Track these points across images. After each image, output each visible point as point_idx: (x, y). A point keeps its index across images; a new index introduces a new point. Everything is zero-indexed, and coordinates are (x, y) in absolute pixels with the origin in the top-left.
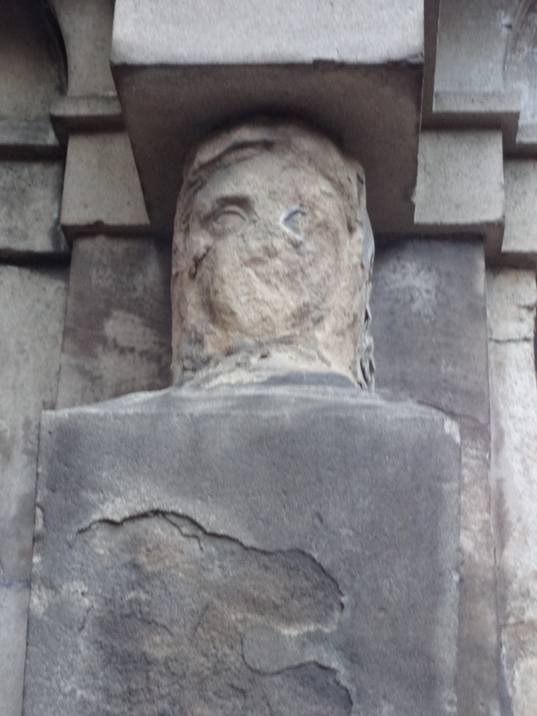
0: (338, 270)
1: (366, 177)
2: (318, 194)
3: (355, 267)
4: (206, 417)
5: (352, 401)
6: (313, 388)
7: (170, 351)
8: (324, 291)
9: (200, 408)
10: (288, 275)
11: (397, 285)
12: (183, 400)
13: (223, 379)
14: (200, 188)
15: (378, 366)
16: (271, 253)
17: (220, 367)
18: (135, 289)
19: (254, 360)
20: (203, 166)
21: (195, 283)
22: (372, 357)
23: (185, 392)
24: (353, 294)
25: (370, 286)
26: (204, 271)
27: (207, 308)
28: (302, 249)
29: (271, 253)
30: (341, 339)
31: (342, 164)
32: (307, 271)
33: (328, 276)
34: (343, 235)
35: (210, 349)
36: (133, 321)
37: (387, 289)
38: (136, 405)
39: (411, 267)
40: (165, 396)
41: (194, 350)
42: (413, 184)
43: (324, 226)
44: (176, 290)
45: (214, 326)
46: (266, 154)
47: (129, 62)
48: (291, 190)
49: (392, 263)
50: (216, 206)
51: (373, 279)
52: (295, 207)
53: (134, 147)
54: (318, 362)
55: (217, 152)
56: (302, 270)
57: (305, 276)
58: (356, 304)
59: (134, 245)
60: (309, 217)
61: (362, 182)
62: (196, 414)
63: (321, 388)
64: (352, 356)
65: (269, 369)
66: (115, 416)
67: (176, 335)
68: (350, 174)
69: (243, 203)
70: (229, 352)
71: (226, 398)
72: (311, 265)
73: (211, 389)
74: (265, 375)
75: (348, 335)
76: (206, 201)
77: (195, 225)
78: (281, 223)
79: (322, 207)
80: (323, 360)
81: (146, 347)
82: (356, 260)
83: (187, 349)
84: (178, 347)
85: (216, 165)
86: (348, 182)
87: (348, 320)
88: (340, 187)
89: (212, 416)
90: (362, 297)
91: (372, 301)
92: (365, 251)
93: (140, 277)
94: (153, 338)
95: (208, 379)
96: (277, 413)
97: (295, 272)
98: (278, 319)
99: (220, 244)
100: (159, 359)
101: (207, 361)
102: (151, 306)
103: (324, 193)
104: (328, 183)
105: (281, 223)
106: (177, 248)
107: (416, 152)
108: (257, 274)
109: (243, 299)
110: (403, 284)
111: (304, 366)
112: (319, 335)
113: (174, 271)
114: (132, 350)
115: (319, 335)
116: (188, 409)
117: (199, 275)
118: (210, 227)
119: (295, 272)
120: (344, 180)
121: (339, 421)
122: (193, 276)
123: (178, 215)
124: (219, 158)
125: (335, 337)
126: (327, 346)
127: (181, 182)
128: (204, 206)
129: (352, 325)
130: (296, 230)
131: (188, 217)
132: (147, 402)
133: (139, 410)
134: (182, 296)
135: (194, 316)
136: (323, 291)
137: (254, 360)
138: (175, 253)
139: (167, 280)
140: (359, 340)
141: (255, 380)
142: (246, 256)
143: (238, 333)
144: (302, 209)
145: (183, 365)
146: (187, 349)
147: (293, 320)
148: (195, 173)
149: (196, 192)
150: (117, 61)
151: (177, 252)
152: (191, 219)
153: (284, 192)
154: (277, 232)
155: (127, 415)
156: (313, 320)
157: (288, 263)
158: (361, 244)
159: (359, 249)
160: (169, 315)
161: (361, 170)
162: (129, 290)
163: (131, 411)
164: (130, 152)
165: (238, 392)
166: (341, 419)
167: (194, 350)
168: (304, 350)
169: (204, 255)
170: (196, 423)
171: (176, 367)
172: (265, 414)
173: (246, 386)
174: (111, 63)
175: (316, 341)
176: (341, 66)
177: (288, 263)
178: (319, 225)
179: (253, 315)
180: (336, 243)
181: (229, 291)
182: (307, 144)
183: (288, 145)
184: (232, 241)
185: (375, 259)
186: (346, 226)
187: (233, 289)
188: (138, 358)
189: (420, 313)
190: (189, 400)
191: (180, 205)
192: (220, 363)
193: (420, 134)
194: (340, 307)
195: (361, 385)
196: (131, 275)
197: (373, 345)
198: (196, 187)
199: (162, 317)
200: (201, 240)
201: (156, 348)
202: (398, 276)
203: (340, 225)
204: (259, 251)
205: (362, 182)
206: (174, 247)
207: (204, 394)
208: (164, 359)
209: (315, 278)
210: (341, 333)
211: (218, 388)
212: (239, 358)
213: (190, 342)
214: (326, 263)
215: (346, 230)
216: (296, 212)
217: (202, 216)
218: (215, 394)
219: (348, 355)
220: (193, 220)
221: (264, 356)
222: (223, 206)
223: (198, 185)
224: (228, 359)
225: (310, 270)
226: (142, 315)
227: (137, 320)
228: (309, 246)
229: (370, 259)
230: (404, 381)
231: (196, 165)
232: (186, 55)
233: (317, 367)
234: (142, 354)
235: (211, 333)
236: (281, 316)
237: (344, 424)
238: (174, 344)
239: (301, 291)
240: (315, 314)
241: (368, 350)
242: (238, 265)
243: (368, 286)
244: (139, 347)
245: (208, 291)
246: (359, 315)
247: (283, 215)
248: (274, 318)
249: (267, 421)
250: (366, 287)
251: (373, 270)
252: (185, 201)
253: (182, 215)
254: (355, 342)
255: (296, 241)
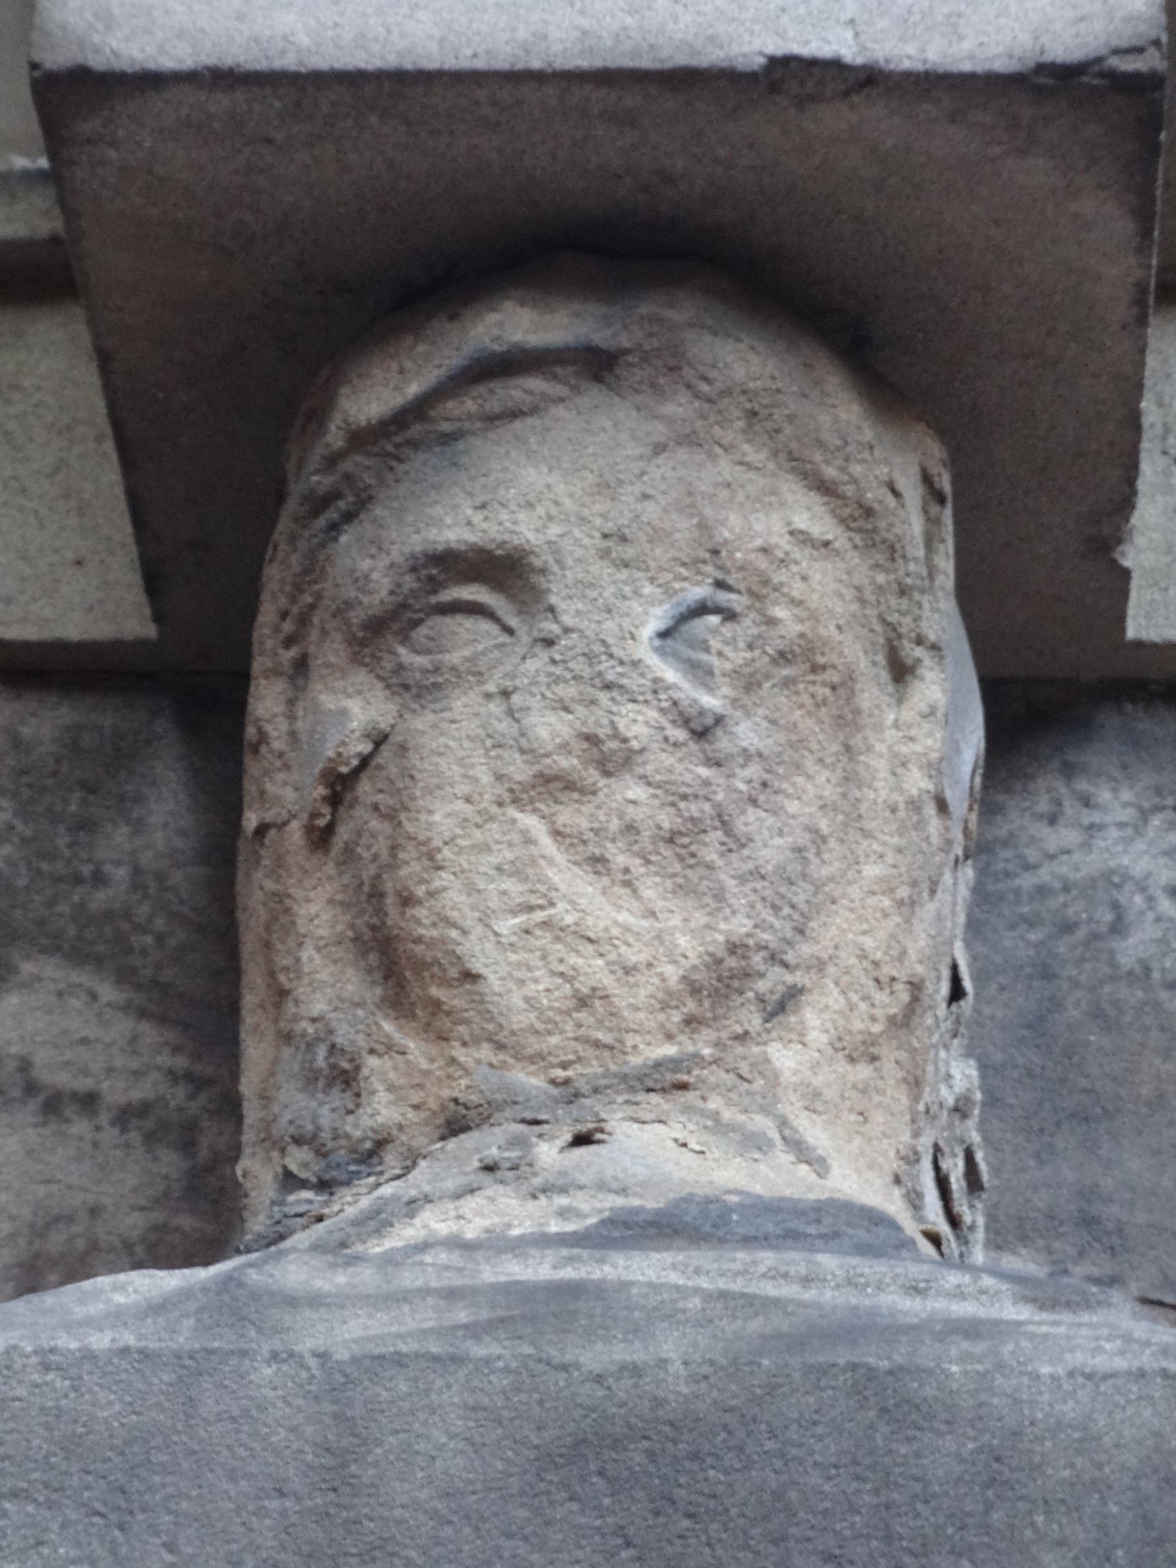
0: (853, 820)
1: (954, 483)
2: (784, 543)
3: (914, 805)
4: (378, 1363)
5: (911, 1307)
6: (767, 1258)
7: (230, 1107)
8: (801, 894)
9: (352, 1333)
10: (671, 840)
11: (1063, 868)
12: (291, 1301)
13: (434, 1222)
14: (349, 517)
15: (996, 1171)
16: (610, 757)
17: (421, 1178)
18: (99, 879)
19: (549, 1153)
20: (362, 439)
21: (330, 869)
22: (975, 1137)
23: (295, 1270)
24: (908, 906)
25: (969, 872)
26: (360, 821)
27: (373, 958)
28: (723, 743)
29: (610, 757)
30: (863, 1072)
31: (868, 435)
32: (740, 827)
33: (820, 839)
34: (872, 691)
35: (382, 1109)
36: (94, 997)
37: (1026, 881)
38: (118, 1317)
39: (1116, 801)
40: (228, 1281)
41: (323, 1110)
42: (1125, 502)
43: (803, 658)
44: (256, 888)
45: (400, 1028)
46: (593, 395)
47: (97, 62)
48: (683, 527)
49: (1047, 787)
50: (410, 582)
51: (978, 850)
52: (699, 591)
53: (105, 359)
54: (785, 1158)
55: (413, 389)
56: (725, 824)
57: (735, 842)
58: (918, 944)
59: (102, 717)
60: (748, 627)
61: (941, 499)
62: (342, 1355)
63: (796, 1260)
64: (906, 1137)
65: (602, 1186)
66: (47, 1360)
67: (256, 1052)
68: (895, 468)
69: (506, 571)
70: (455, 1124)
71: (452, 1295)
72: (754, 802)
73: (390, 1261)
74: (592, 1208)
75: (890, 1054)
76: (370, 563)
77: (330, 651)
78: (644, 649)
79: (797, 589)
80: (801, 1150)
81: (140, 1093)
82: (917, 782)
83: (296, 1105)
84: (265, 1098)
85: (406, 432)
86: (891, 501)
87: (890, 1003)
88: (861, 519)
89: (399, 1360)
90: (939, 918)
91: (975, 928)
92: (953, 747)
93: (120, 835)
94: (164, 1060)
95: (377, 1221)
96: (638, 1354)
97: (697, 828)
98: (634, 1000)
99: (421, 722)
100: (186, 1137)
101: (371, 1154)
102: (160, 938)
103: (800, 537)
104: (814, 498)
105: (644, 649)
106: (263, 737)
107: (1137, 388)
108: (557, 834)
109: (507, 925)
110: (1089, 863)
111: (729, 1174)
112: (785, 1058)
113: (251, 820)
114: (88, 1102)
115: (785, 1058)
116: (313, 1335)
117: (343, 833)
118: (388, 664)
119: (697, 828)
120: (875, 494)
121: (865, 1381)
122: (321, 838)
123: (267, 613)
124: (419, 409)
125: (843, 1067)
126: (813, 1099)
127: (280, 497)
128: (363, 582)
129: (903, 1022)
130: (701, 673)
131: (304, 620)
132: (158, 1308)
133: (129, 1339)
134: (280, 903)
135: (326, 984)
136: (796, 894)
137: (549, 1153)
138: (255, 749)
139: (222, 845)
140: (930, 1076)
141: (554, 1227)
142: (520, 770)
143: (485, 1052)
144: (723, 597)
145: (285, 1167)
146: (296, 1105)
147: (691, 1006)
148: (332, 461)
149: (334, 528)
150: (56, 59)
151: (263, 749)
152: (314, 634)
153: (658, 535)
154: (633, 682)
155: (88, 1355)
156: (761, 999)
157: (674, 795)
158: (935, 723)
159: (929, 741)
160: (229, 972)
161: (936, 450)
162: (78, 880)
163: (100, 1341)
164: (89, 375)
165: (491, 1272)
166: (872, 1374)
167: (323, 1110)
168: (727, 1115)
169: (365, 761)
170: (340, 1384)
171: (257, 1172)
172: (596, 1356)
173: (519, 1246)
174: (34, 66)
175: (774, 1080)
176: (868, 80)
177: (674, 795)
178: (783, 657)
179: (541, 984)
180: (847, 720)
181: (455, 899)
182: (743, 360)
183: (670, 366)
184: (466, 707)
185: (986, 776)
186: (881, 658)
187: (471, 889)
188: (110, 1135)
189: (1147, 970)
190: (316, 1301)
191: (274, 575)
192: (423, 1164)
193: (1152, 320)
194: (863, 956)
195: (935, 1239)
196: (85, 826)
197: (978, 1096)
198: (332, 514)
199: (202, 987)
200: (352, 709)
201: (178, 1095)
202: (1066, 836)
203: (857, 654)
204: (564, 747)
205: (941, 499)
206: (251, 732)
207: (366, 1277)
208: (210, 1139)
209: (771, 851)
210: (863, 1052)
211: (418, 1258)
212: (489, 1142)
213: (310, 1079)
214: (809, 794)
215: (885, 676)
216: (701, 609)
217: (356, 617)
218: (409, 1278)
219: (890, 1131)
220: (324, 632)
221: (582, 1140)
222: (434, 585)
223: (343, 507)
224: (452, 1144)
225: (749, 821)
226: (124, 976)
227: (108, 992)
228: (747, 733)
229: (967, 778)
230: (1089, 1222)
231: (334, 437)
232: (304, 40)
233: (776, 1177)
234: (125, 1116)
235: (390, 1048)
236: (646, 989)
237: (884, 1389)
238: (248, 1085)
239: (719, 896)
240: (772, 981)
241: (960, 1110)
242: (487, 802)
243: (960, 874)
244: (116, 1092)
245: (377, 895)
246: (930, 987)
247: (656, 619)
248: (622, 1000)
249: (599, 1379)
250: (956, 878)
251: (980, 814)
252: (295, 561)
253: (284, 615)
254: (915, 1084)
255: (702, 713)
